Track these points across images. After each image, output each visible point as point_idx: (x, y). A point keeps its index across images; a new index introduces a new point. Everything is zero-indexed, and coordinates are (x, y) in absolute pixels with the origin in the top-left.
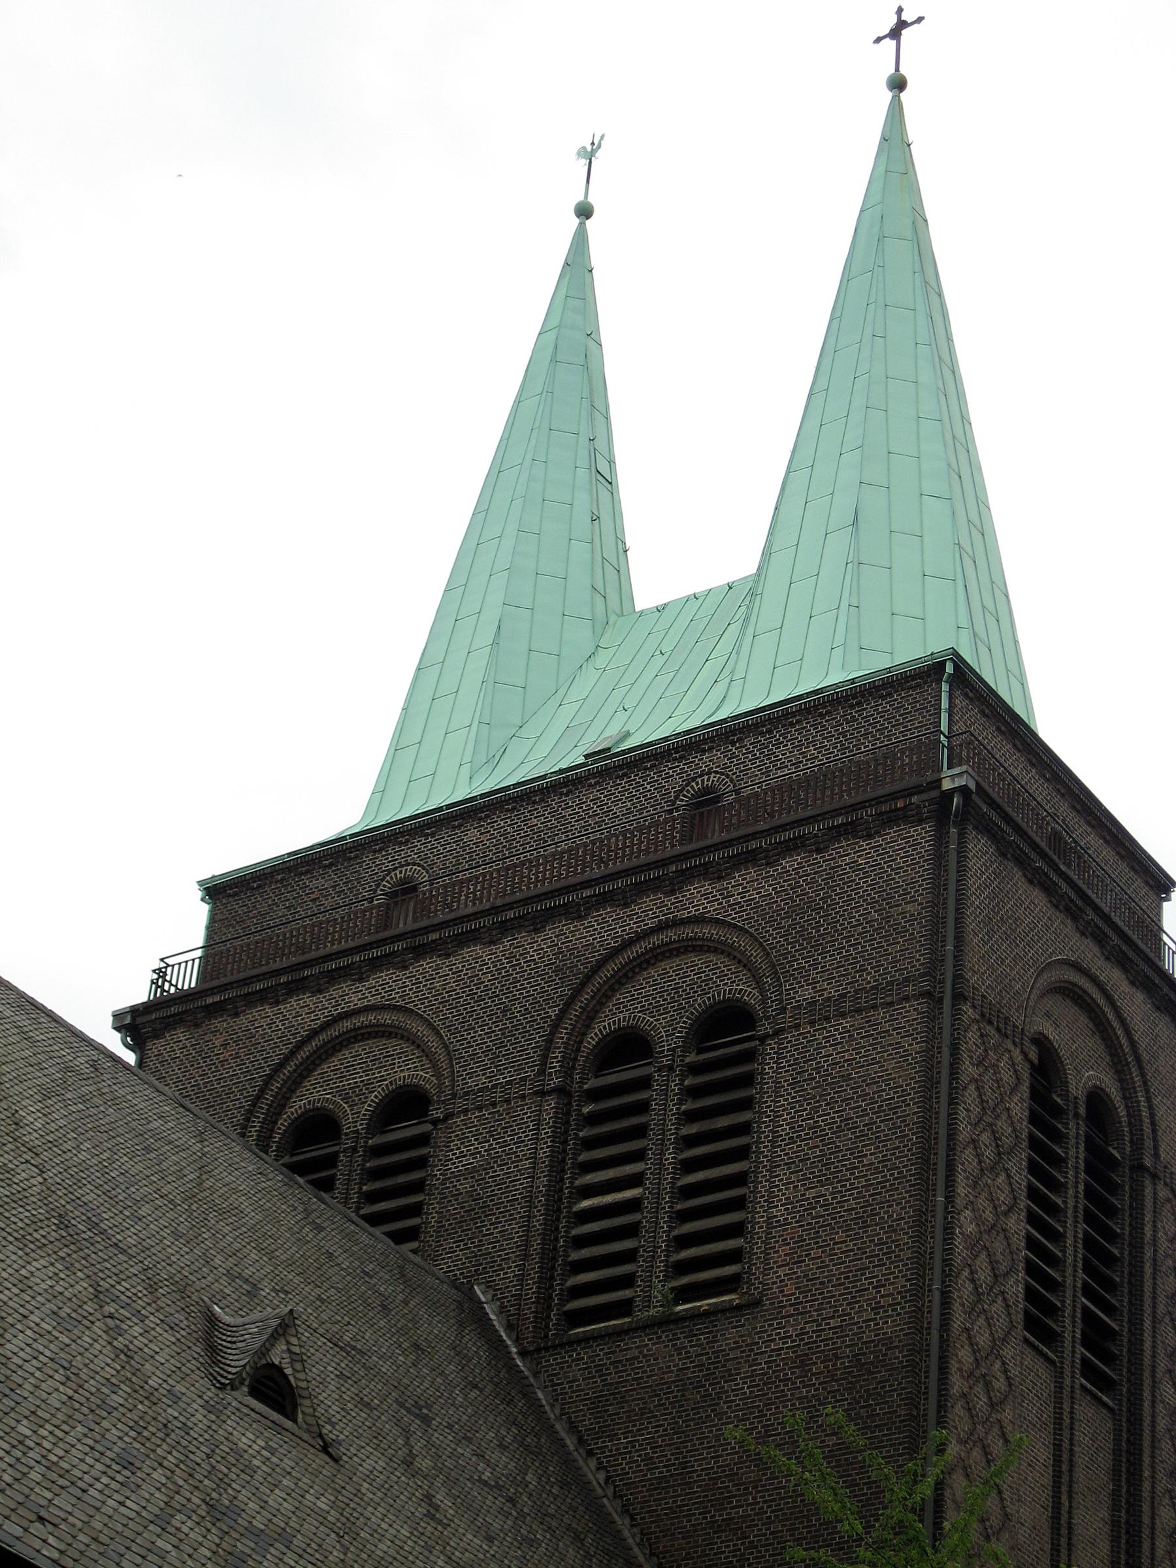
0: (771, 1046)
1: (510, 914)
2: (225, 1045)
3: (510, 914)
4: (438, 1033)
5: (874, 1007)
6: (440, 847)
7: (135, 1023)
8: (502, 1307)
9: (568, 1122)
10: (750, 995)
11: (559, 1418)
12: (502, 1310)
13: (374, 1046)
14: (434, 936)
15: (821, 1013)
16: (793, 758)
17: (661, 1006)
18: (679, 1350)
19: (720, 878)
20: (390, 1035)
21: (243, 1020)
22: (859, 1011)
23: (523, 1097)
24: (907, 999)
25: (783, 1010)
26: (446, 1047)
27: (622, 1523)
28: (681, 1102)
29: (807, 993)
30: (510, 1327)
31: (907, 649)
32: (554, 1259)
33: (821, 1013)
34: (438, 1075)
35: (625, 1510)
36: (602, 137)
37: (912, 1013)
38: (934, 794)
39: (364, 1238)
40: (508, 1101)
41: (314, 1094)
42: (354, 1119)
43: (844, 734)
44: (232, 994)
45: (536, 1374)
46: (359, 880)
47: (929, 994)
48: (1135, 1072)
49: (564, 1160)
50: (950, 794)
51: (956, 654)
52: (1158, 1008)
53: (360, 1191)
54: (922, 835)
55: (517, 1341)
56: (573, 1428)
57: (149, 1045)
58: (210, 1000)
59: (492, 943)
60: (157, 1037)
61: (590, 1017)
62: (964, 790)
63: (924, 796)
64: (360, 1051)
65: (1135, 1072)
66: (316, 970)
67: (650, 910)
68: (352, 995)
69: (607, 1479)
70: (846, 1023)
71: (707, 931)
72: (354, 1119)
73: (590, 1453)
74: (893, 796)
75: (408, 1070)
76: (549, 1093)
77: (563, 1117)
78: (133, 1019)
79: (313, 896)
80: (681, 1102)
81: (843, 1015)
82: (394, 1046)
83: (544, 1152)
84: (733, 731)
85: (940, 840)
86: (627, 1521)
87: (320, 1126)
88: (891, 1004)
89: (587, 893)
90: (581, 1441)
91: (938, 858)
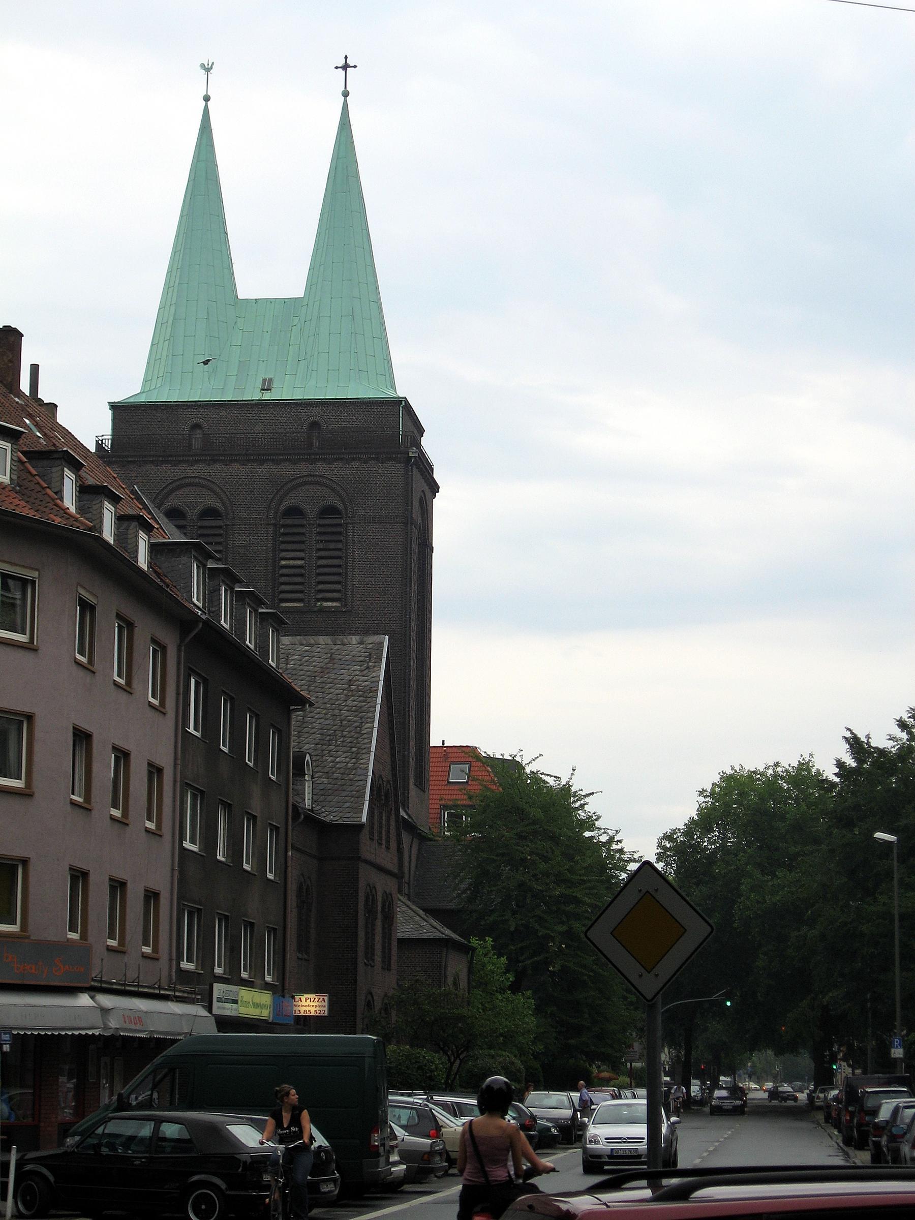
0: (350, 527)
10: (341, 506)
17: (309, 499)
34: (223, 503)
67: (303, 469)
70: (377, 526)
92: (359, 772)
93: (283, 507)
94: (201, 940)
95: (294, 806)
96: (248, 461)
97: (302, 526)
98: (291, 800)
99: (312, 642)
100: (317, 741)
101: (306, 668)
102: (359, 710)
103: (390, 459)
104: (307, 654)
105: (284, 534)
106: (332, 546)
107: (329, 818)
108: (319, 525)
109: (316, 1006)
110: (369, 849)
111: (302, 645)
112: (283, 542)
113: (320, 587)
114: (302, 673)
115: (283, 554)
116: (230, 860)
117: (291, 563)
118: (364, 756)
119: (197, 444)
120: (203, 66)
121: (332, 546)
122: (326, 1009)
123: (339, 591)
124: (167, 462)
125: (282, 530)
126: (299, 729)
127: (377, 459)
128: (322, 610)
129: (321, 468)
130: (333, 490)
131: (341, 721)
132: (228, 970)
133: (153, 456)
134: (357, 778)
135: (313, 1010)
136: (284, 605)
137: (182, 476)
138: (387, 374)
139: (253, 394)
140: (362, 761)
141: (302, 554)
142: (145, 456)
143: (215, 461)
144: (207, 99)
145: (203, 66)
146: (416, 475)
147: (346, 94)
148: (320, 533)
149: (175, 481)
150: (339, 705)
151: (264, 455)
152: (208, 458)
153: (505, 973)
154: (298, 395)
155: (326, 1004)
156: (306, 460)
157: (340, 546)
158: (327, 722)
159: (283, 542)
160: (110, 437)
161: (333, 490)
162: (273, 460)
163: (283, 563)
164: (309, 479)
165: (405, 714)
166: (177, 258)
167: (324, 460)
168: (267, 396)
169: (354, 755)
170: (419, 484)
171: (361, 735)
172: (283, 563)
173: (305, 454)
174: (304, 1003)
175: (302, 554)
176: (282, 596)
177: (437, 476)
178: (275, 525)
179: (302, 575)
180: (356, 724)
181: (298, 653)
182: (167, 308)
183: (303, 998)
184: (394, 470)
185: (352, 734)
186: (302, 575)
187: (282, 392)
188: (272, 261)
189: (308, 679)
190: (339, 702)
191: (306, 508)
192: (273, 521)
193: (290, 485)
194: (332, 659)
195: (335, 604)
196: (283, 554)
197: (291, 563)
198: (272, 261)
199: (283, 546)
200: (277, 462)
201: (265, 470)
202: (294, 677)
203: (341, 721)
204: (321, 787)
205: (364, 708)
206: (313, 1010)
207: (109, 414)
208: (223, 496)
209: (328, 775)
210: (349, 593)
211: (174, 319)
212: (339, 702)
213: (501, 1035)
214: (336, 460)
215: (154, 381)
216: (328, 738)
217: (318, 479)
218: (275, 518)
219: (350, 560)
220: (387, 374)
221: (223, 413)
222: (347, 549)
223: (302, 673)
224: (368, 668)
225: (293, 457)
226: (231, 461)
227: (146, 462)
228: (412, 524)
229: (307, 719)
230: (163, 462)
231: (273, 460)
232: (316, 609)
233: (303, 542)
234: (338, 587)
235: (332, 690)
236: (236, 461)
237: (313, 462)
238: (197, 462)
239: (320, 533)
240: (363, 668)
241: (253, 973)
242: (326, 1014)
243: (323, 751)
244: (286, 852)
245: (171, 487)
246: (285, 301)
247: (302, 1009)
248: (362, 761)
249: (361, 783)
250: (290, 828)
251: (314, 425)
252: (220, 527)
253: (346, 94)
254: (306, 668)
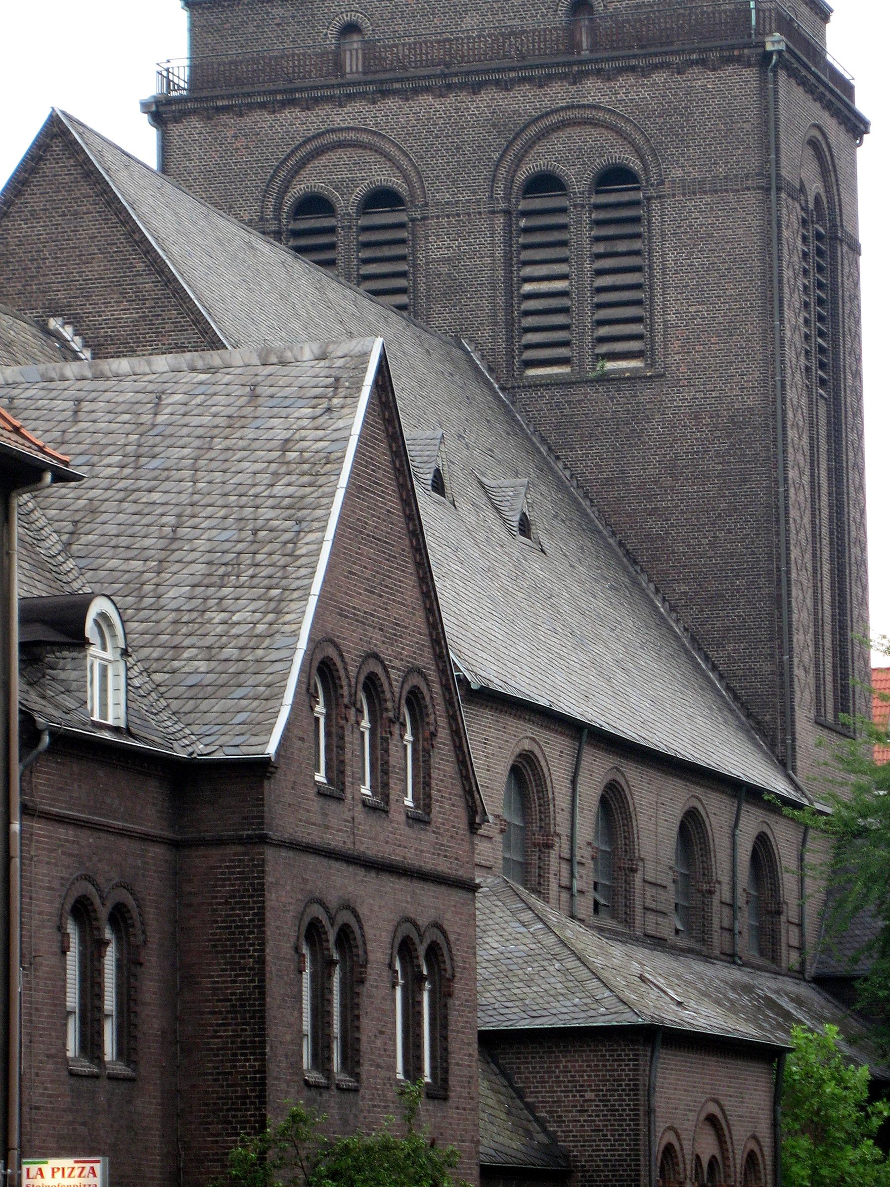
0: (655, 205)
2: (235, 137)
4: (407, 156)
5: (726, 191)
7: (161, 112)
8: (483, 356)
9: (511, 232)
10: (635, 164)
11: (533, 433)
12: (483, 357)
13: (355, 154)
17: (573, 157)
18: (612, 399)
20: (365, 148)
22: (716, 191)
23: (480, 213)
24: (748, 189)
25: (662, 183)
26: (416, 168)
27: (585, 504)
29: (679, 173)
30: (491, 370)
32: (513, 325)
34: (406, 178)
35: (586, 496)
37: (752, 199)
38: (760, 50)
39: (858, 687)
40: (469, 214)
44: (238, 101)
45: (513, 403)
46: (313, 16)
47: (761, 188)
48: (832, 174)
49: (511, 259)
50: (771, 53)
52: (840, 124)
53: (357, 257)
55: (497, 380)
56: (543, 440)
57: (170, 126)
58: (220, 103)
59: (441, 96)
60: (176, 122)
61: (519, 160)
62: (779, 52)
63: (753, 51)
65: (832, 174)
66: (305, 95)
67: (558, 94)
69: (572, 475)
70: (708, 198)
71: (601, 115)
72: (346, 203)
73: (558, 458)
74: (732, 48)
75: (383, 176)
76: (498, 212)
78: (157, 107)
79: (276, 21)
80: (591, 229)
81: (705, 193)
82: (370, 157)
83: (499, 253)
85: (763, 81)
86: (588, 503)
87: (315, 204)
88: (738, 191)
90: (550, 449)
91: (762, 90)
93: (521, 176)
96: (450, 87)
97: (563, 210)
100: (197, 579)
101: (196, 421)
104: (202, 388)
105: (527, 230)
106: (622, 246)
108: (598, 207)
112: (526, 247)
113: (603, 331)
114: (185, 431)
115: (528, 271)
117: (544, 287)
118: (293, 606)
121: (622, 246)
124: (292, 103)
125: (523, 223)
126: (163, 554)
127: (703, 63)
128: (605, 379)
129: (593, 91)
130: (619, 132)
131: (255, 532)
133: (264, 93)
136: (531, 372)
140: (288, 618)
141: (562, 268)
142: (249, 95)
148: (599, 223)
152: (371, 88)
156: (563, 77)
157: (637, 245)
158: (226, 535)
159: (526, 247)
161: (619, 132)
162: (497, 83)
163: (528, 288)
164: (570, 114)
165: (779, 581)
167: (599, 73)
169: (272, 605)
172: (528, 288)
173: (558, 65)
175: (562, 268)
176: (530, 354)
177: (861, 104)
178: (507, 212)
179: (565, 310)
181: (185, 388)
185: (275, 557)
186: (565, 310)
189: (197, 443)
190: (258, 489)
192: (503, 205)
193: (533, 130)
194: (254, 396)
196: (528, 271)
197: (544, 287)
199: (526, 255)
200: (505, 86)
202: (169, 442)
203: (255, 532)
204: (192, 680)
205: (308, 501)
208: (405, 163)
210: (659, 339)
212: (258, 489)
214: (621, 71)
216: (223, 570)
217: (588, 114)
219: (657, 273)
223: (185, 431)
224: (329, 410)
225: (536, 73)
226: (416, 91)
227: (251, 107)
228: (779, 189)
229: (181, 532)
230: (284, 104)
233: (564, 244)
235: (245, 465)
236: (427, 90)
237: (576, 78)
238: (350, 97)
239: (599, 223)
240: (318, 411)
243: (206, 599)
245: (300, 154)
249: (278, 666)
254: (196, 421)
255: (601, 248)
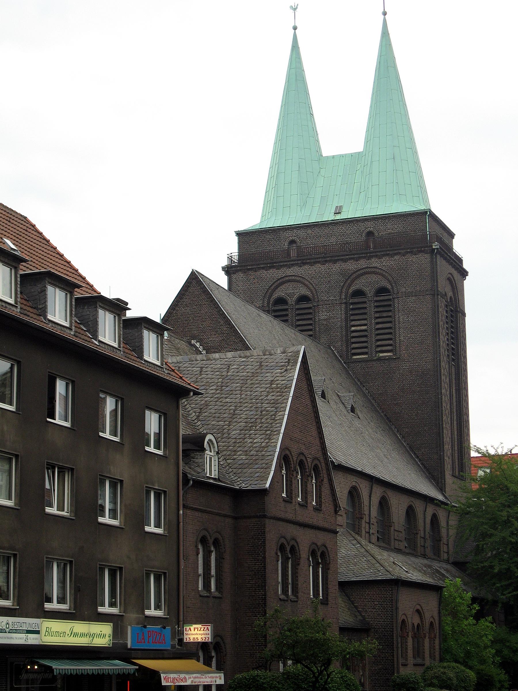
0: (396, 301)
1: (328, 259)
3: (328, 259)
6: (301, 233)
10: (389, 287)
12: (338, 352)
14: (309, 261)
15: (408, 295)
16: (391, 228)
17: (367, 284)
19: (380, 258)
21: (258, 273)
28: (374, 309)
30: (341, 356)
31: (468, 270)
33: (408, 295)
34: (312, 293)
36: (298, 5)
38: (431, 248)
41: (279, 293)
42: (292, 301)
43: (403, 224)
51: (430, 210)
54: (428, 256)
58: (249, 267)
61: (350, 286)
63: (428, 248)
64: (291, 284)
67: (362, 263)
68: (290, 272)
70: (414, 298)
75: (304, 291)
77: (346, 308)
80: (374, 309)
84: (376, 218)
85: (432, 258)
87: (281, 301)
89: (347, 257)
91: (431, 261)
92: (270, 449)
93: (351, 291)
94: (123, 585)
95: (185, 475)
96: (326, 261)
97: (365, 302)
98: (181, 468)
99: (248, 354)
101: (241, 374)
102: (276, 402)
103: (421, 251)
104: (243, 363)
105: (352, 309)
106: (385, 314)
107: (244, 486)
108: (376, 301)
109: (202, 634)
110: (274, 507)
111: (240, 357)
112: (352, 315)
113: (379, 343)
114: (238, 378)
115: (353, 323)
116: (73, 514)
117: (359, 328)
118: (275, 437)
119: (293, 254)
120: (291, 7)
121: (385, 314)
122: (209, 636)
123: (391, 345)
124: (273, 267)
125: (351, 307)
127: (411, 252)
128: (380, 359)
129: (375, 263)
131: (261, 412)
132: (72, 606)
134: (268, 454)
135: (199, 637)
136: (355, 357)
137: (284, 275)
138: (421, 196)
139: (329, 216)
140: (273, 441)
141: (365, 322)
143: (304, 264)
144: (295, 28)
145: (291, 7)
146: (441, 263)
147: (385, 14)
149: (279, 279)
150: (262, 400)
151: (336, 256)
152: (300, 262)
153: (472, 604)
154: (358, 214)
155: (209, 632)
157: (390, 314)
158: (252, 413)
159: (352, 315)
160: (237, 254)
162: (342, 260)
163: (353, 328)
166: (279, 134)
168: (338, 217)
169: (268, 436)
170: (444, 268)
171: (275, 420)
172: (353, 328)
174: (193, 632)
175: (365, 322)
176: (353, 351)
178: (346, 303)
179: (366, 336)
180: (272, 413)
182: (274, 166)
183: (192, 628)
184: (424, 259)
186: (366, 336)
187: (347, 214)
188: (342, 127)
190: (262, 397)
191: (366, 289)
193: (355, 275)
195: (389, 354)
197: (359, 328)
198: (342, 127)
199: (352, 318)
200: (345, 261)
201: (336, 267)
203: (261, 412)
204: (240, 462)
206: (199, 637)
207: (236, 239)
208: (311, 287)
209: (246, 453)
211: (278, 173)
212: (262, 397)
213: (349, 653)
215: (267, 216)
218: (346, 298)
219: (397, 323)
220: (421, 196)
221: (309, 231)
222: (395, 316)
223: (238, 378)
224: (286, 370)
227: (260, 269)
228: (438, 295)
229: (237, 412)
230: (270, 268)
231: (342, 260)
232: (375, 358)
234: (391, 342)
237: (369, 258)
241: (122, 609)
242: (210, 640)
244: (179, 511)
246: (352, 155)
247: (192, 637)
248: (273, 441)
249: (270, 457)
250: (181, 493)
251: (370, 234)
252: (310, 308)
253: (385, 14)
255: (377, 315)
